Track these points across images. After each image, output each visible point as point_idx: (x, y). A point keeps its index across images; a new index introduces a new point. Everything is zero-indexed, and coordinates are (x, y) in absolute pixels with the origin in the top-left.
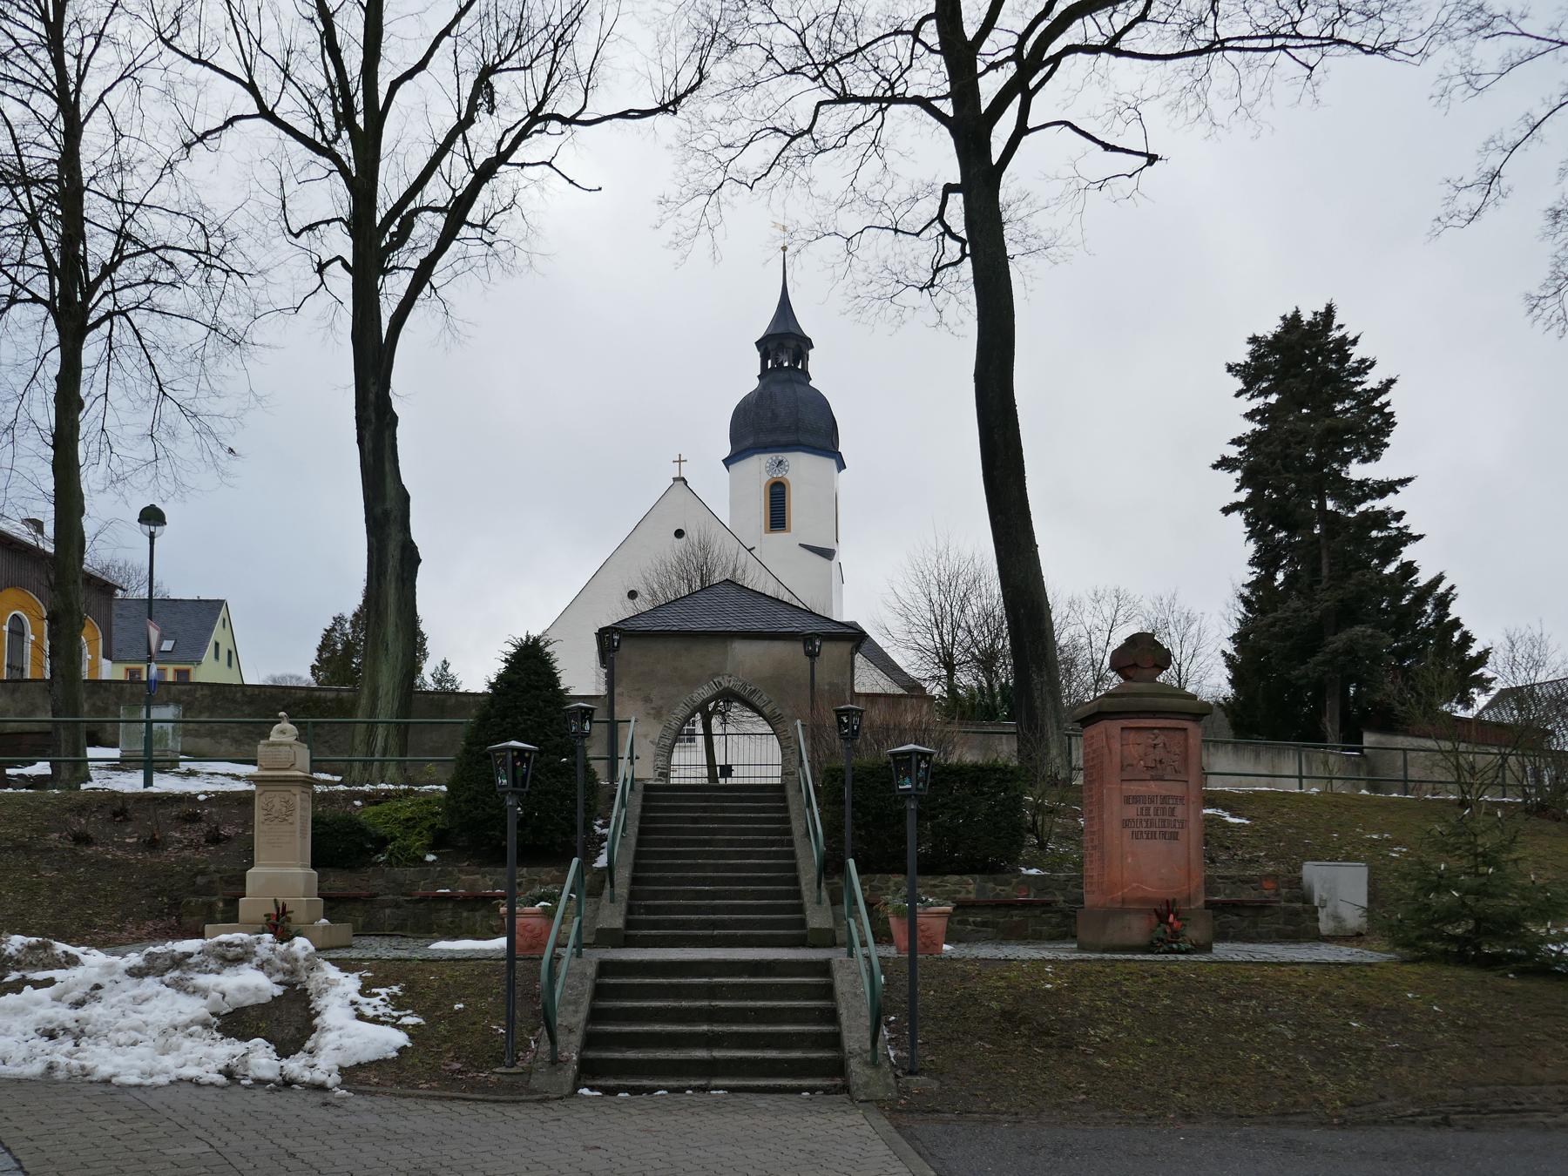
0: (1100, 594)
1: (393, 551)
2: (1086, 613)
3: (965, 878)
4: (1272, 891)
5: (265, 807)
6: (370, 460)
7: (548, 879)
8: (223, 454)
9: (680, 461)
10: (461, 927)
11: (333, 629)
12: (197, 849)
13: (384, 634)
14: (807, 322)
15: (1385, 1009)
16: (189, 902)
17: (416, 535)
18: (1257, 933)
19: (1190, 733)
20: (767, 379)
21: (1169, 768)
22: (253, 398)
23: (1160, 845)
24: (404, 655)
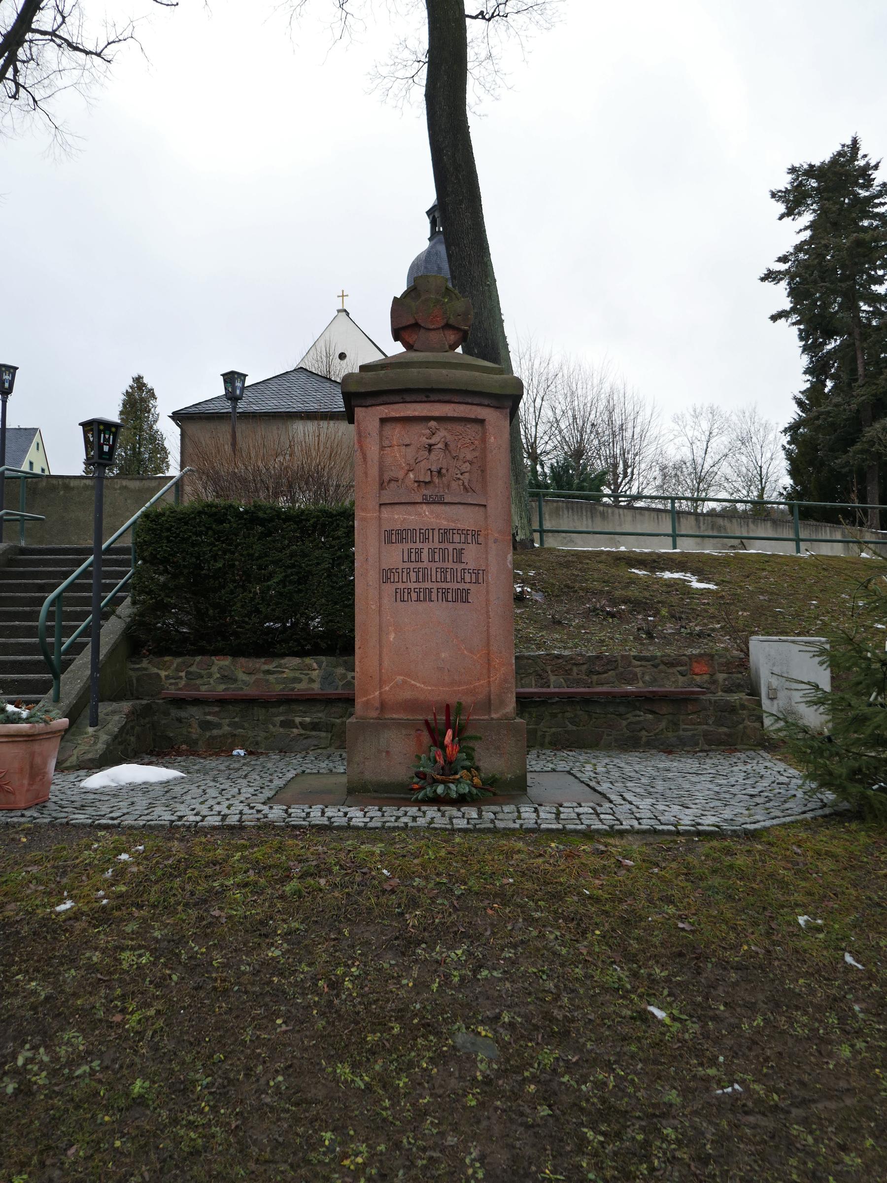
0: (698, 411)
2: (688, 428)
3: (308, 660)
4: (706, 677)
9: (343, 296)
15: (738, 968)
19: (489, 427)
21: (454, 485)
23: (438, 610)
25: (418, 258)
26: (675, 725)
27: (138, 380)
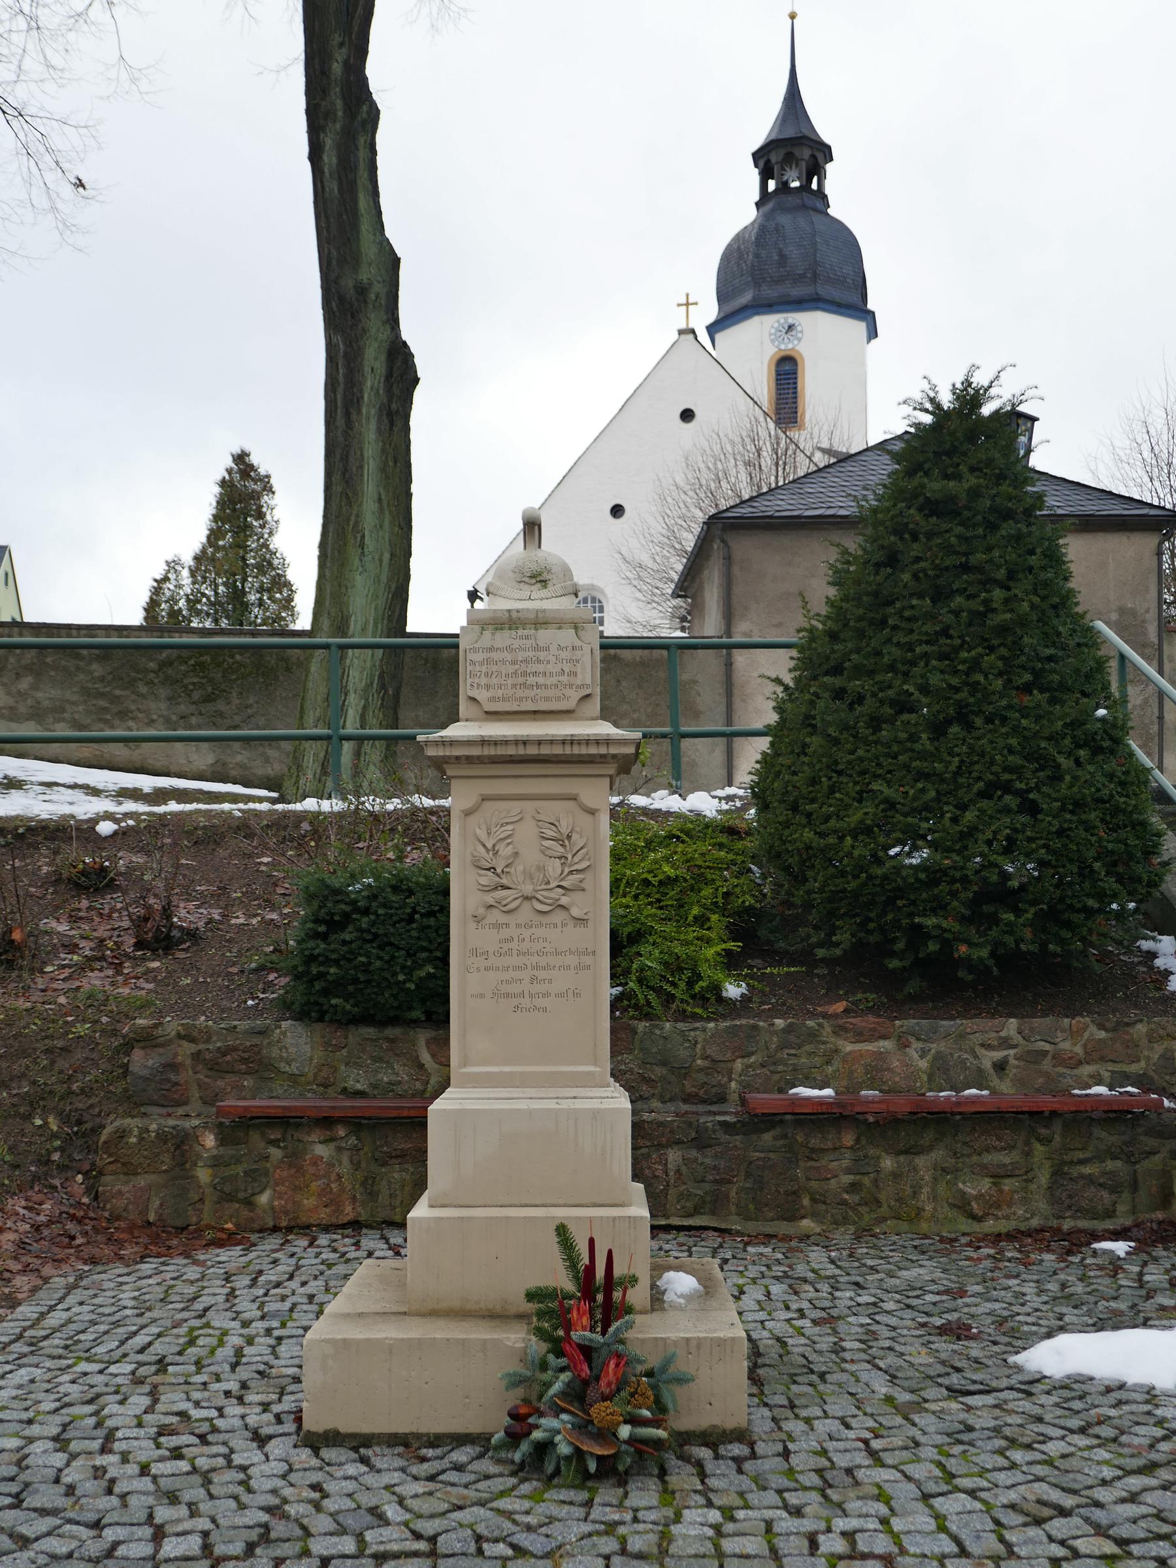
1: (373, 360)
5: (487, 858)
6: (333, 186)
7: (1078, 1049)
8: (68, 190)
9: (687, 304)
10: (878, 1203)
11: (166, 579)
12: (118, 968)
13: (357, 516)
14: (825, 128)
16: (122, 1134)
17: (408, 332)
22: (124, 76)
24: (392, 555)
25: (738, 238)
26: (357, 1245)
27: (241, 458)
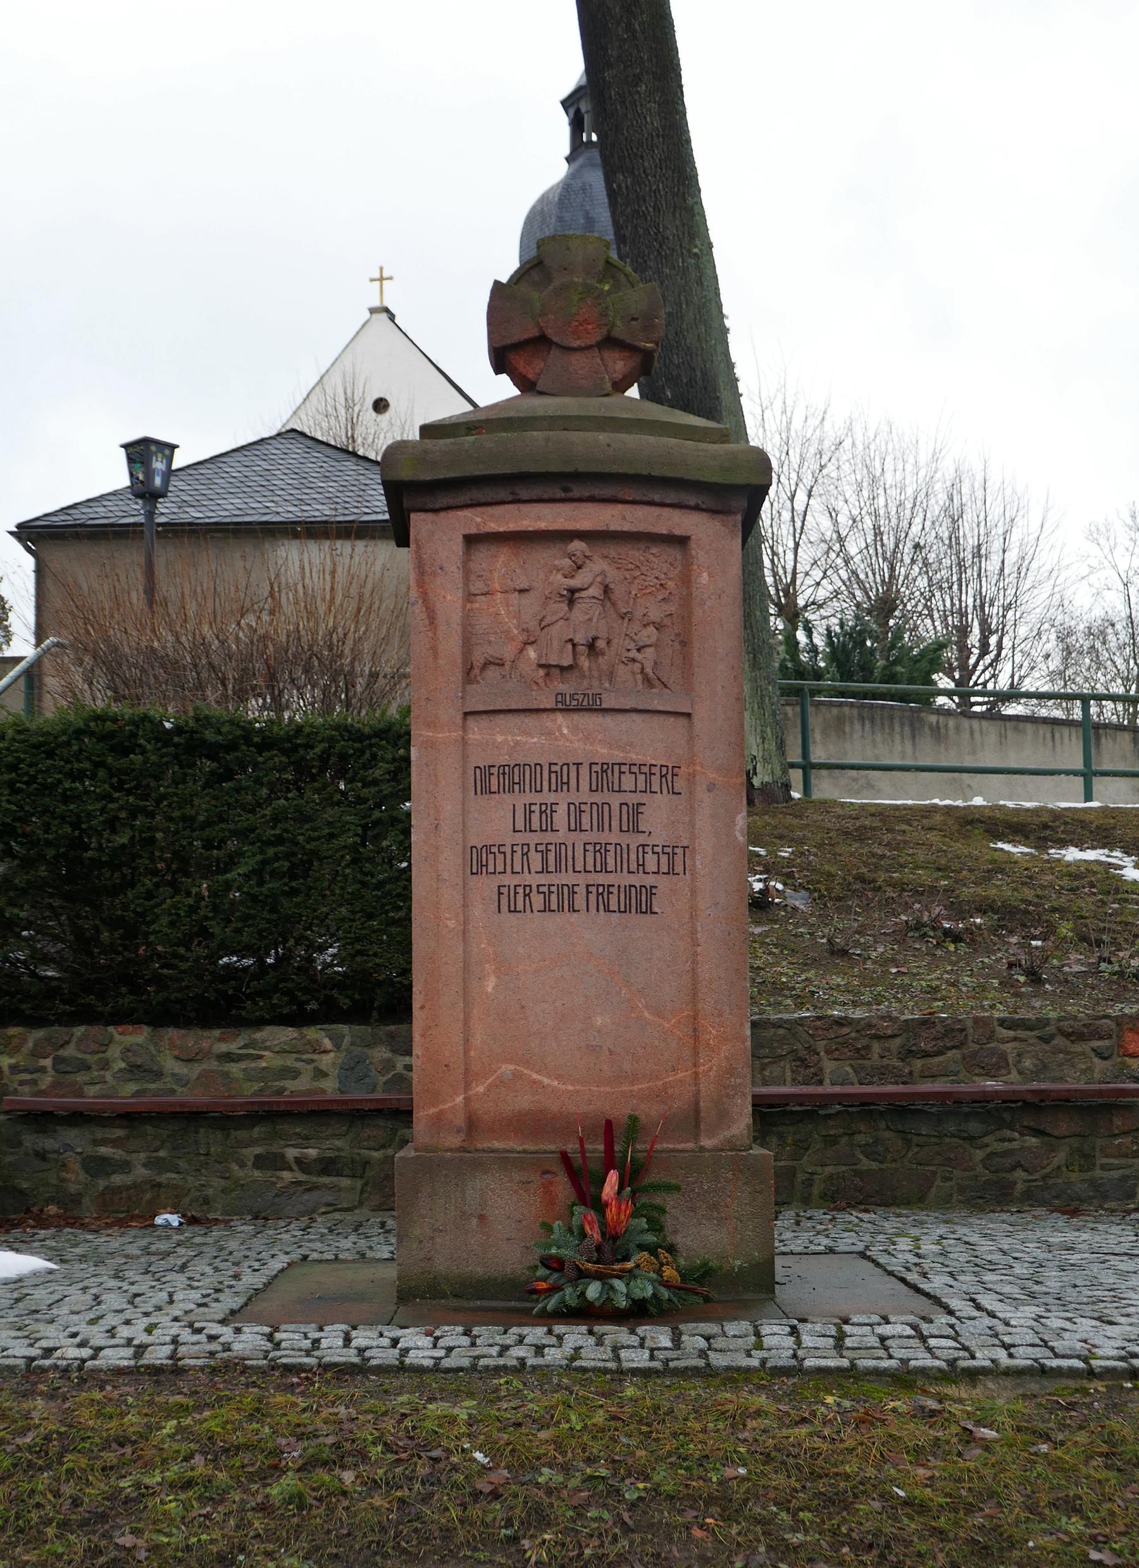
3: (312, 1033)
9: (381, 279)
18: (1094, 1184)
19: (700, 555)
20: (580, 161)
21: (622, 672)
25: (544, 199)
